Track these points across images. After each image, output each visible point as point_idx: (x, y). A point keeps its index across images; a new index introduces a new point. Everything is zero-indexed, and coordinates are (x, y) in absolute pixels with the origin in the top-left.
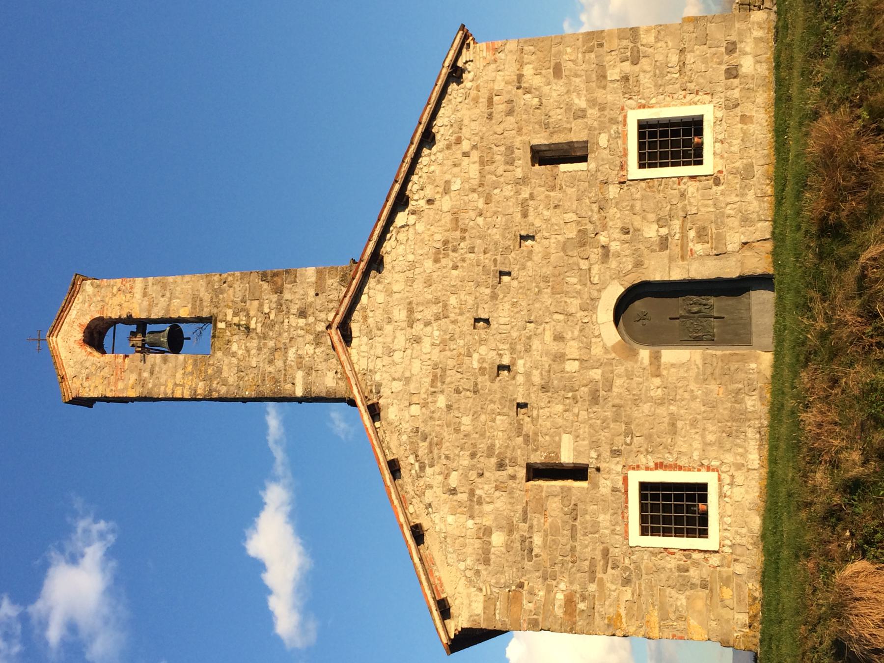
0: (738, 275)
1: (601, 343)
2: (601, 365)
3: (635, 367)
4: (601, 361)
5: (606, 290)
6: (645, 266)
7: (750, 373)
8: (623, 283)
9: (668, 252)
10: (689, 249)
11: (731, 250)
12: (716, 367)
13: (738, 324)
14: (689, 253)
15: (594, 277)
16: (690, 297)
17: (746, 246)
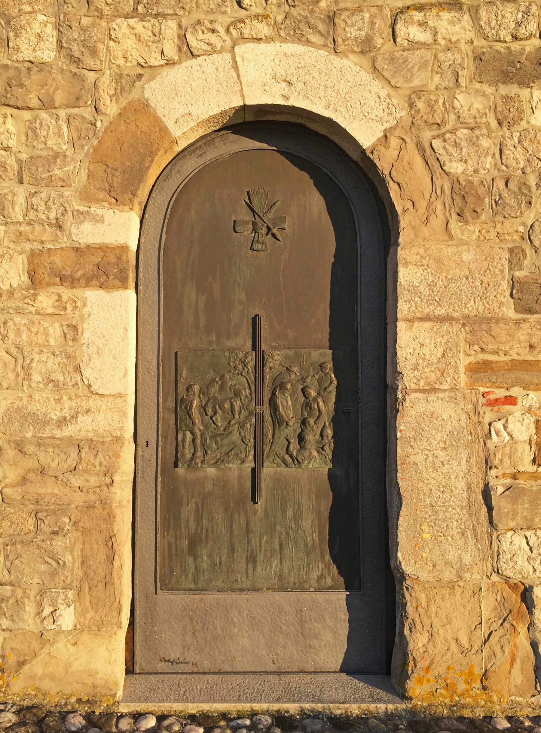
0: (407, 569)
1: (155, 60)
2: (70, 57)
3: (67, 193)
4: (89, 61)
5: (365, 76)
6: (455, 225)
7: (40, 605)
8: (394, 142)
9: (510, 312)
10: (515, 392)
11: (505, 546)
12: (66, 484)
13: (232, 549)
14: (501, 393)
15: (423, 24)
16: (333, 388)
17: (515, 598)
